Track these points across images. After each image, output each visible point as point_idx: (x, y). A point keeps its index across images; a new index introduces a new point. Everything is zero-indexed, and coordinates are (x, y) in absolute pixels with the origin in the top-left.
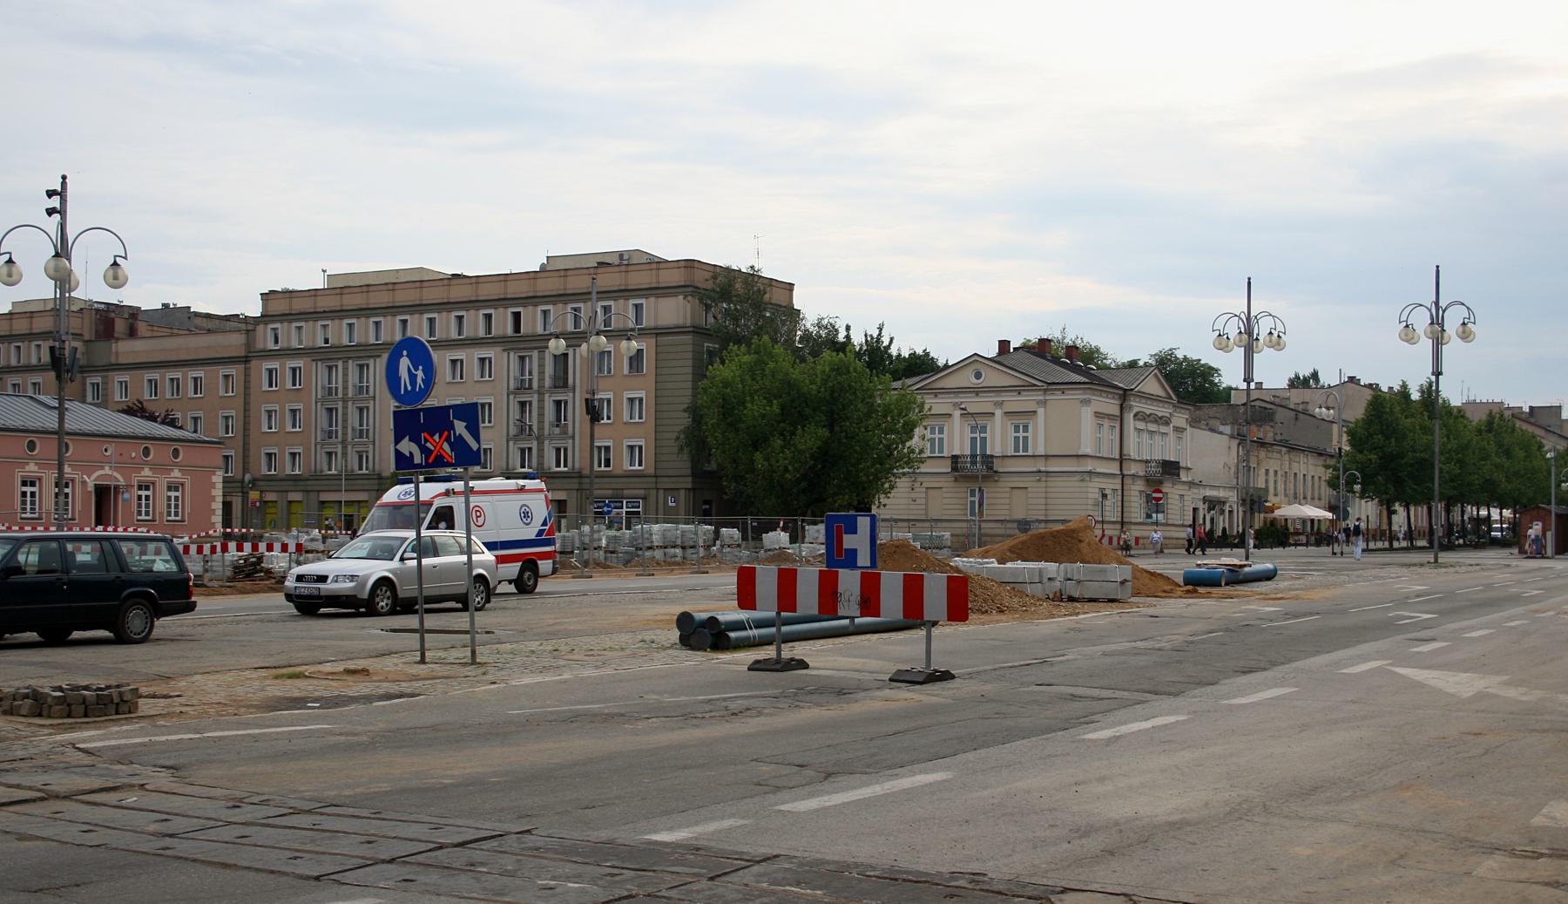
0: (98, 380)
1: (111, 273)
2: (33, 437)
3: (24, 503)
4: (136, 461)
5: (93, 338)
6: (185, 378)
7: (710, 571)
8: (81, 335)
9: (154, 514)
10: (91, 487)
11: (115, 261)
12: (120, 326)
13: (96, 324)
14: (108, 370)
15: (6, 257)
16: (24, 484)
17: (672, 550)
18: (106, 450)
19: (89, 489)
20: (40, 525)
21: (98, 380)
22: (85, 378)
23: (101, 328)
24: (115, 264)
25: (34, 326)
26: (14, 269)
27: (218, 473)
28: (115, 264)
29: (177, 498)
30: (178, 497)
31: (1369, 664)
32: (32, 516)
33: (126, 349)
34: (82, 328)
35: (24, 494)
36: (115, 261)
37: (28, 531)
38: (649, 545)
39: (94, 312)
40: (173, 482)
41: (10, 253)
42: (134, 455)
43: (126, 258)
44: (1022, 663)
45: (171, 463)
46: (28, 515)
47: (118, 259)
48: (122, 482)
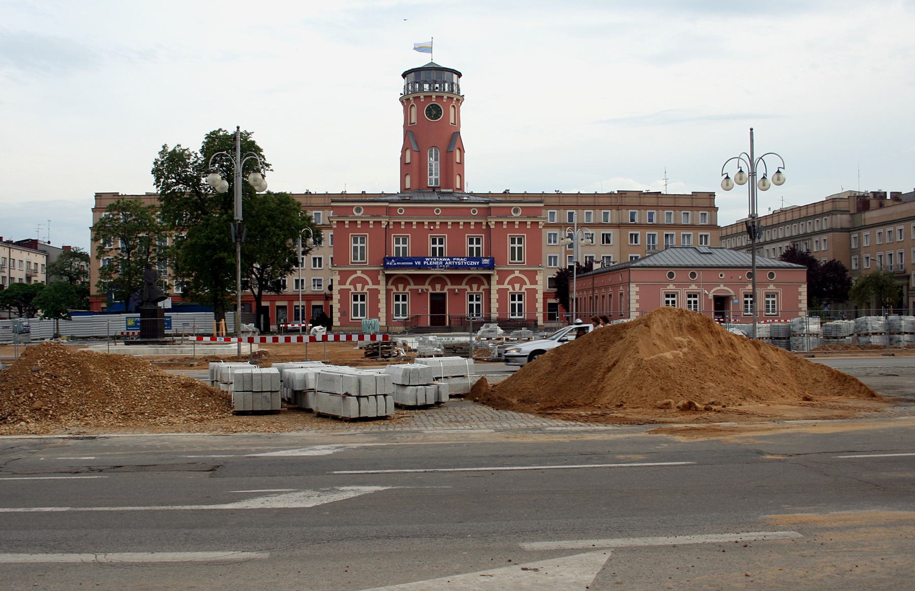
0: (856, 235)
1: (738, 176)
2: (671, 270)
3: (768, 307)
4: (742, 281)
5: (856, 212)
6: (885, 232)
7: (896, 354)
8: (848, 211)
9: (778, 312)
10: (711, 296)
11: (778, 170)
12: (874, 203)
13: (857, 205)
14: (859, 229)
15: (726, 176)
16: (667, 296)
17: (897, 336)
18: (721, 275)
19: (710, 298)
20: (777, 319)
21: (856, 235)
22: (850, 235)
23: (861, 206)
24: (778, 172)
25: (817, 210)
26: (766, 182)
27: (803, 286)
28: (778, 172)
29: (773, 302)
30: (774, 301)
31: (281, 505)
32: (773, 314)
33: (871, 216)
34: (849, 208)
35: (768, 302)
36: (778, 170)
37: (776, 322)
38: (865, 332)
39: (856, 198)
40: (770, 292)
41: (727, 173)
42: (740, 277)
43: (784, 168)
44: (60, 436)
45: (767, 281)
46: (771, 313)
47: (780, 169)
48: (732, 293)
